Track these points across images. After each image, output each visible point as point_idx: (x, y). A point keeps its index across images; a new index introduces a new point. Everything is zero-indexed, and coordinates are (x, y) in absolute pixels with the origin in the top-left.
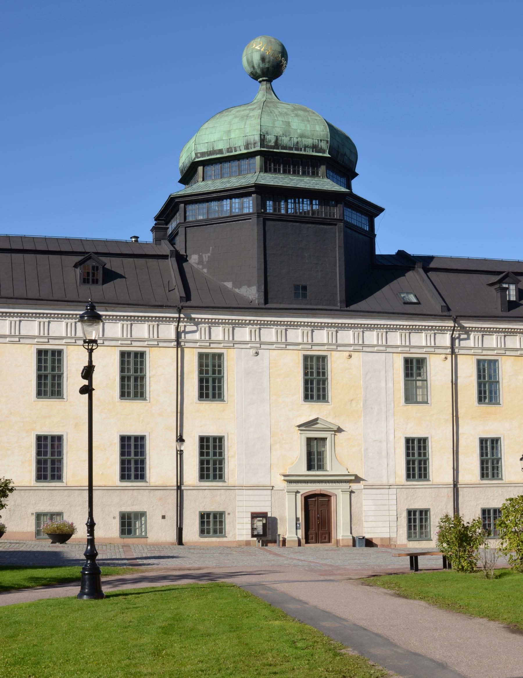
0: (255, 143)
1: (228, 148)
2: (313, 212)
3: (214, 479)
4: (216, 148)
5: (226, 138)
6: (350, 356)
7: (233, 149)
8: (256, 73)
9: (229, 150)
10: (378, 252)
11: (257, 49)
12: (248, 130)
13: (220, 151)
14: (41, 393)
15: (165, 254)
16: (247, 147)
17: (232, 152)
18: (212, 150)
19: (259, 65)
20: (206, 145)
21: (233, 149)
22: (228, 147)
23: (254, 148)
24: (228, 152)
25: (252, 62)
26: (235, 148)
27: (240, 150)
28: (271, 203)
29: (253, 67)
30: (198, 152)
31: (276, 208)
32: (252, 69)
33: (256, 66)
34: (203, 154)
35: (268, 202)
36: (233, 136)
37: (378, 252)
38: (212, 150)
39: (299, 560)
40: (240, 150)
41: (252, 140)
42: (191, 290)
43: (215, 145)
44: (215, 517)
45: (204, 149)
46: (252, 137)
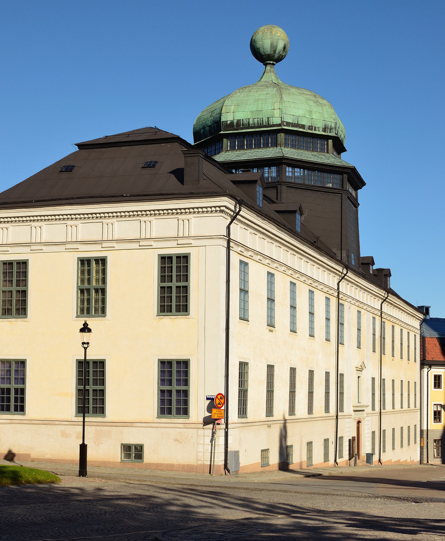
0: (331, 129)
2: (295, 177)
3: (177, 414)
4: (300, 123)
5: (309, 117)
7: (314, 128)
8: (274, 56)
9: (310, 128)
11: (273, 37)
12: (326, 116)
13: (303, 126)
14: (184, 364)
16: (324, 130)
17: (312, 130)
21: (314, 128)
23: (330, 132)
24: (309, 129)
26: (315, 128)
27: (319, 131)
29: (275, 51)
31: (293, 173)
32: (272, 52)
34: (288, 124)
39: (296, 492)
40: (319, 131)
41: (329, 126)
44: (136, 448)
45: (289, 120)
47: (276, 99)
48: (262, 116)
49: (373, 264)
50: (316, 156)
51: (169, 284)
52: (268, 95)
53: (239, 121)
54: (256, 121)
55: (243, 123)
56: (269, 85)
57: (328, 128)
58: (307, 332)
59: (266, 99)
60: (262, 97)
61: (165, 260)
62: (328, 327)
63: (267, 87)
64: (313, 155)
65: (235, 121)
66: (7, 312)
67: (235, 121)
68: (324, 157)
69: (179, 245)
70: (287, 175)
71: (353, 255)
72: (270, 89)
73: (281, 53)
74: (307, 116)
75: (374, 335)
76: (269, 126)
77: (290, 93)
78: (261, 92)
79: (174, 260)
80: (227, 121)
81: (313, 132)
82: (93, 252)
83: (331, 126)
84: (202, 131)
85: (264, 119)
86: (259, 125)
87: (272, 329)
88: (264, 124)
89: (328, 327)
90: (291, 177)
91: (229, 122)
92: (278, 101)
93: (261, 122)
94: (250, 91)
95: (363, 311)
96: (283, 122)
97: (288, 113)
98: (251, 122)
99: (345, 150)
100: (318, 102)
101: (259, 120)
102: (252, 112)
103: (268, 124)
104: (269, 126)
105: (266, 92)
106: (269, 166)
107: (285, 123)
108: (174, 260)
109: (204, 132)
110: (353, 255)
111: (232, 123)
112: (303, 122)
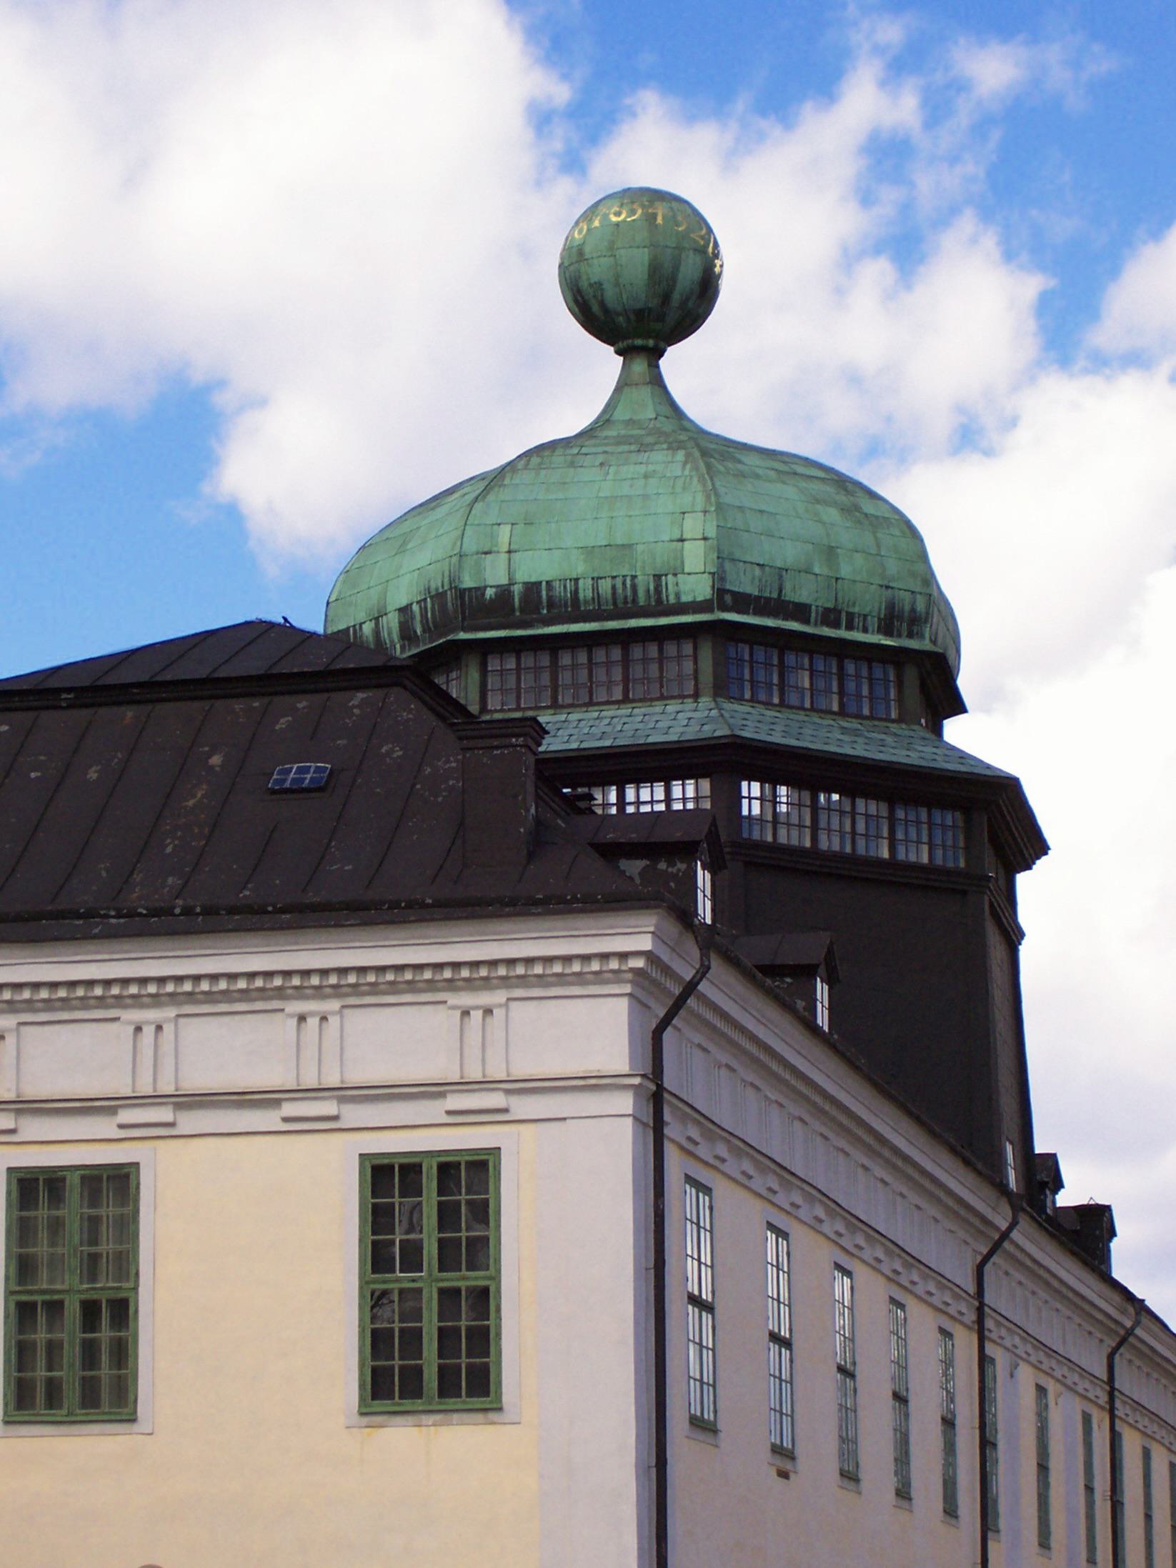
1: (827, 610)
4: (790, 595)
5: (825, 571)
6: (703, 1426)
9: (831, 617)
10: (1037, 1151)
13: (800, 612)
15: (805, 961)
17: (836, 625)
18: (775, 595)
19: (684, 302)
20: (757, 571)
22: (830, 605)
25: (673, 279)
26: (850, 616)
28: (756, 788)
29: (666, 298)
30: (728, 587)
32: (654, 303)
33: (676, 297)
35: (744, 784)
36: (845, 571)
37: (1037, 1151)
38: (775, 595)
41: (907, 608)
42: (626, 1027)
43: (788, 587)
46: (907, 597)
47: (686, 500)
48: (633, 567)
49: (1058, 1184)
50: (855, 732)
51: (452, 1280)
52: (651, 481)
53: (532, 589)
54: (605, 586)
55: (550, 598)
56: (650, 440)
57: (900, 617)
58: (890, 1483)
59: (645, 497)
60: (626, 490)
61: (387, 1179)
62: (950, 1448)
63: (643, 448)
64: (844, 730)
65: (517, 589)
66: (36, 1399)
67: (517, 589)
68: (889, 740)
69: (460, 1117)
70: (745, 812)
71: (1009, 1148)
72: (659, 457)
73: (690, 304)
74: (817, 570)
75: (1089, 1489)
76: (662, 608)
77: (743, 475)
78: (624, 469)
79: (430, 1183)
80: (481, 590)
81: (842, 633)
82: (424, 1134)
83: (913, 610)
84: (368, 629)
85: (640, 580)
86: (620, 605)
87: (788, 1466)
88: (642, 601)
89: (950, 1448)
90: (761, 819)
91: (490, 593)
92: (699, 507)
93: (629, 592)
94: (572, 465)
95: (1051, 1387)
96: (720, 592)
97: (738, 555)
98: (586, 591)
99: (963, 710)
100: (857, 508)
101: (619, 582)
102: (589, 551)
103: (659, 601)
104: (662, 608)
105: (642, 469)
106: (770, 778)
107: (728, 598)
108: (430, 1183)
109: (377, 632)
110: (1009, 1148)
111: (504, 593)
112: (801, 591)
